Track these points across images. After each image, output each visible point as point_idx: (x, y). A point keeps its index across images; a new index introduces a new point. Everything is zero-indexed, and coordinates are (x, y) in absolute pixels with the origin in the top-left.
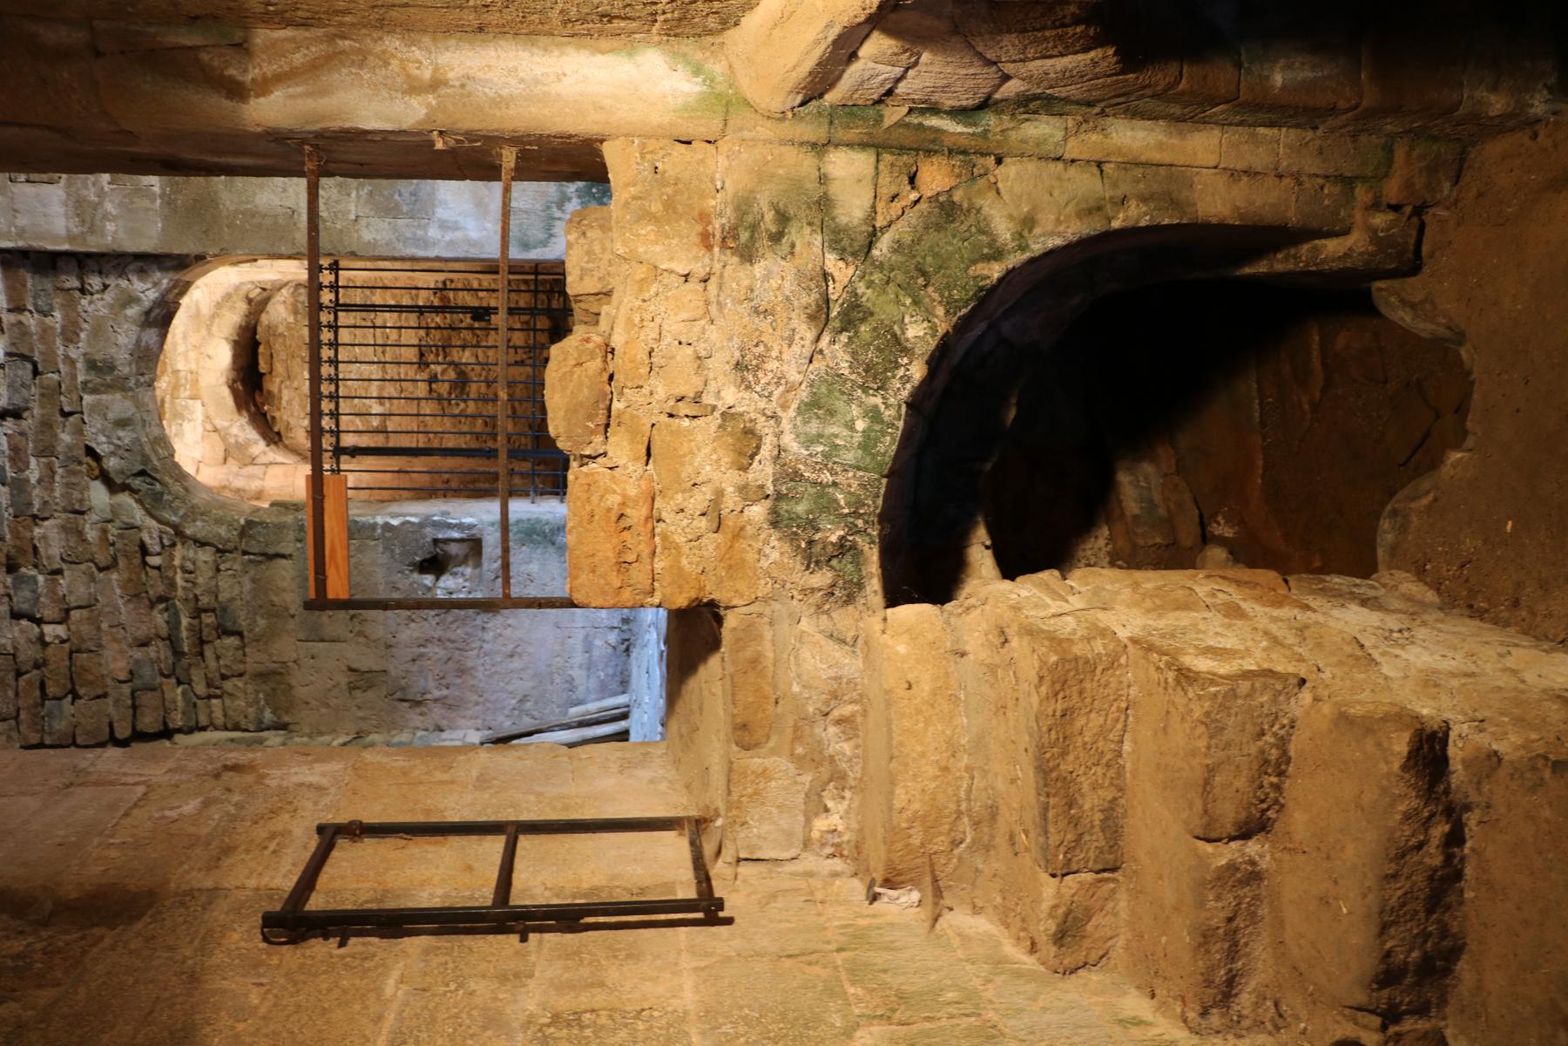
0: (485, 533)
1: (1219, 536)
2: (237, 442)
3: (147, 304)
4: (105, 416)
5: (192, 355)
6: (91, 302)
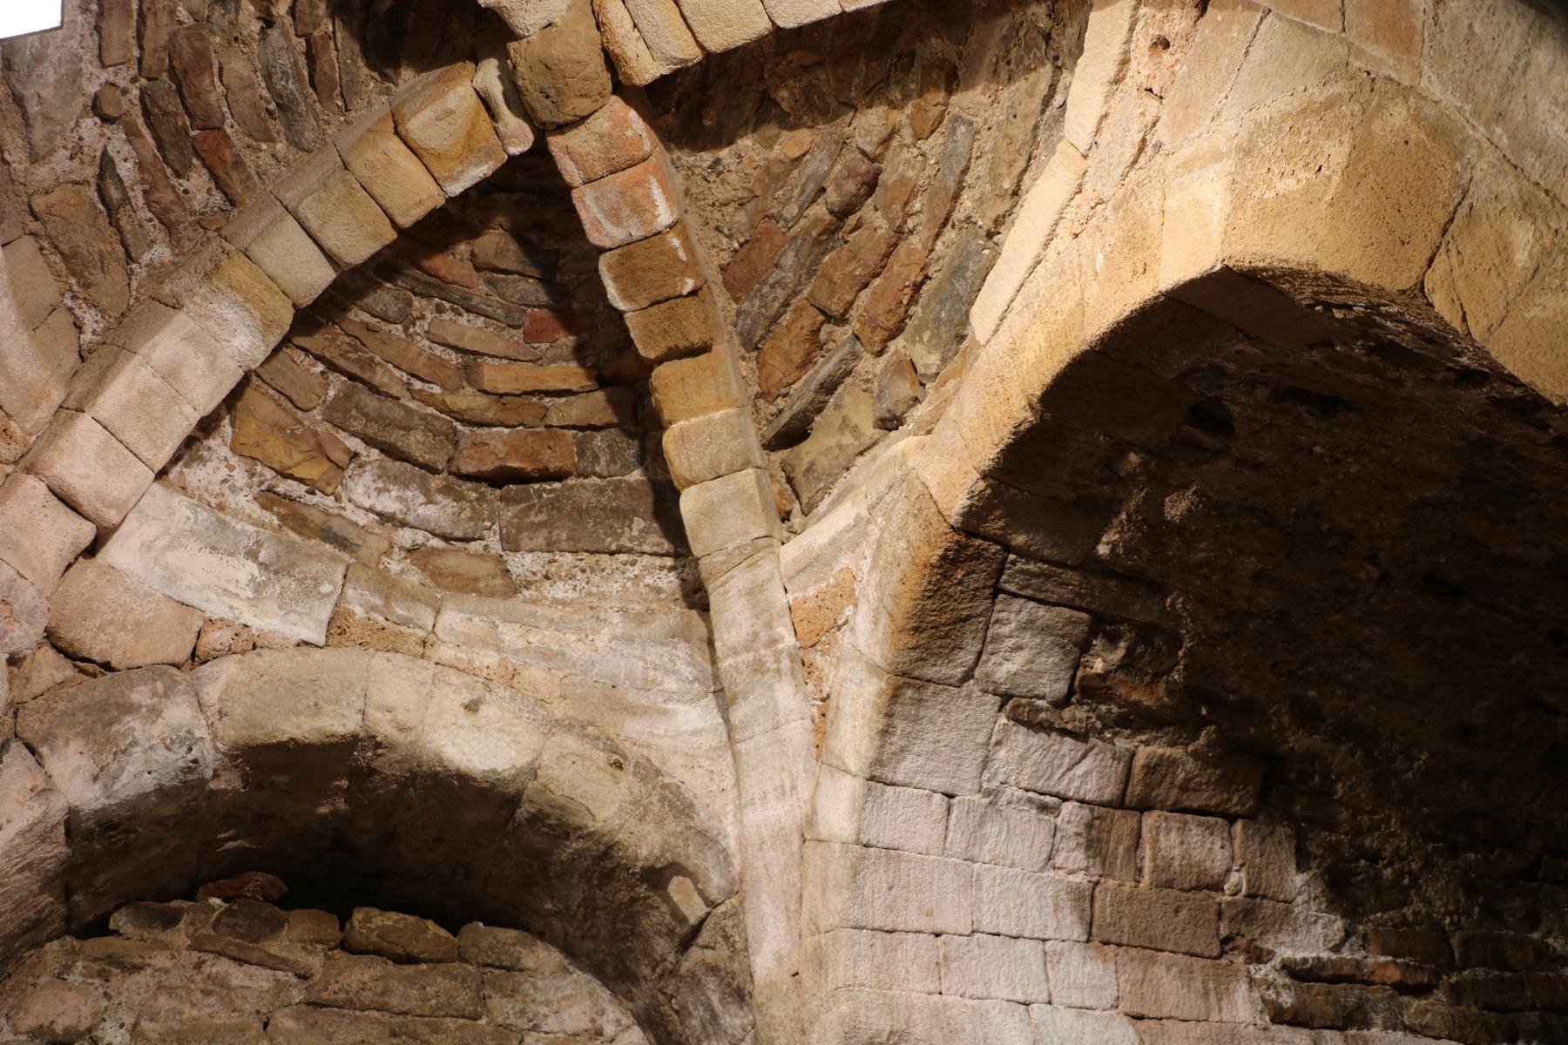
2: (129, 709)
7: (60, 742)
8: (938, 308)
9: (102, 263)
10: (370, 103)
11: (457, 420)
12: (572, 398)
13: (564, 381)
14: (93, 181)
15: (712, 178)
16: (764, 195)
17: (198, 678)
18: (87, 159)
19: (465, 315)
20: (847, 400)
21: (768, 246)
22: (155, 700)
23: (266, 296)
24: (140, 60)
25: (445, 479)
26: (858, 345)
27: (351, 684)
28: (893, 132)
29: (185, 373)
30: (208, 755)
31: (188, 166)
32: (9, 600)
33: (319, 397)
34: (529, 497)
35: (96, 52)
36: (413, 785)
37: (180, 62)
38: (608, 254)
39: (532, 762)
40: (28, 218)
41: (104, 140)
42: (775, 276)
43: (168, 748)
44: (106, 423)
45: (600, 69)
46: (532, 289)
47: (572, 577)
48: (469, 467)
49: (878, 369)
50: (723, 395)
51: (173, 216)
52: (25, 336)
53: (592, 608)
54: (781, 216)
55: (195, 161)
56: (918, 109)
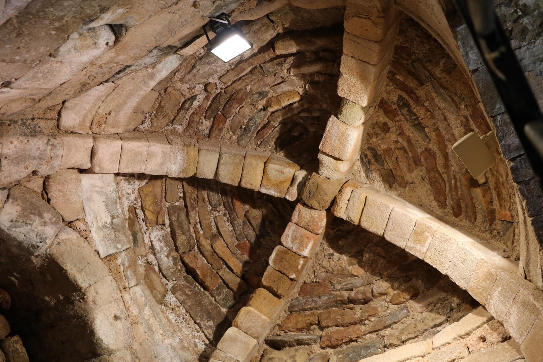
1: (234, 300)
2: (40, 215)
7: (16, 203)
8: (351, 352)
9: (165, 116)
10: (266, 150)
11: (197, 245)
12: (231, 273)
13: (234, 266)
14: (186, 98)
15: (327, 257)
16: (335, 275)
17: (64, 229)
18: (191, 92)
19: (229, 223)
20: (301, 351)
21: (323, 289)
22: (49, 221)
23: (192, 164)
24: (228, 86)
25: (177, 256)
26: (319, 340)
27: (96, 275)
28: (385, 294)
29: (153, 159)
30: (43, 249)
31: (209, 118)
32: (53, 159)
33: (173, 201)
34: (192, 284)
35: (221, 75)
36: (77, 319)
37: (236, 96)
38: (282, 246)
39: (112, 350)
40: (163, 90)
41: (199, 93)
42: (316, 299)
43: (37, 235)
44: (123, 148)
45: (329, 201)
46: (252, 235)
47: (179, 317)
48: (186, 260)
49: (318, 352)
50: (271, 313)
51: (193, 124)
52: (131, 111)
53: (174, 330)
54: (334, 285)
55: (212, 119)
56: (398, 294)
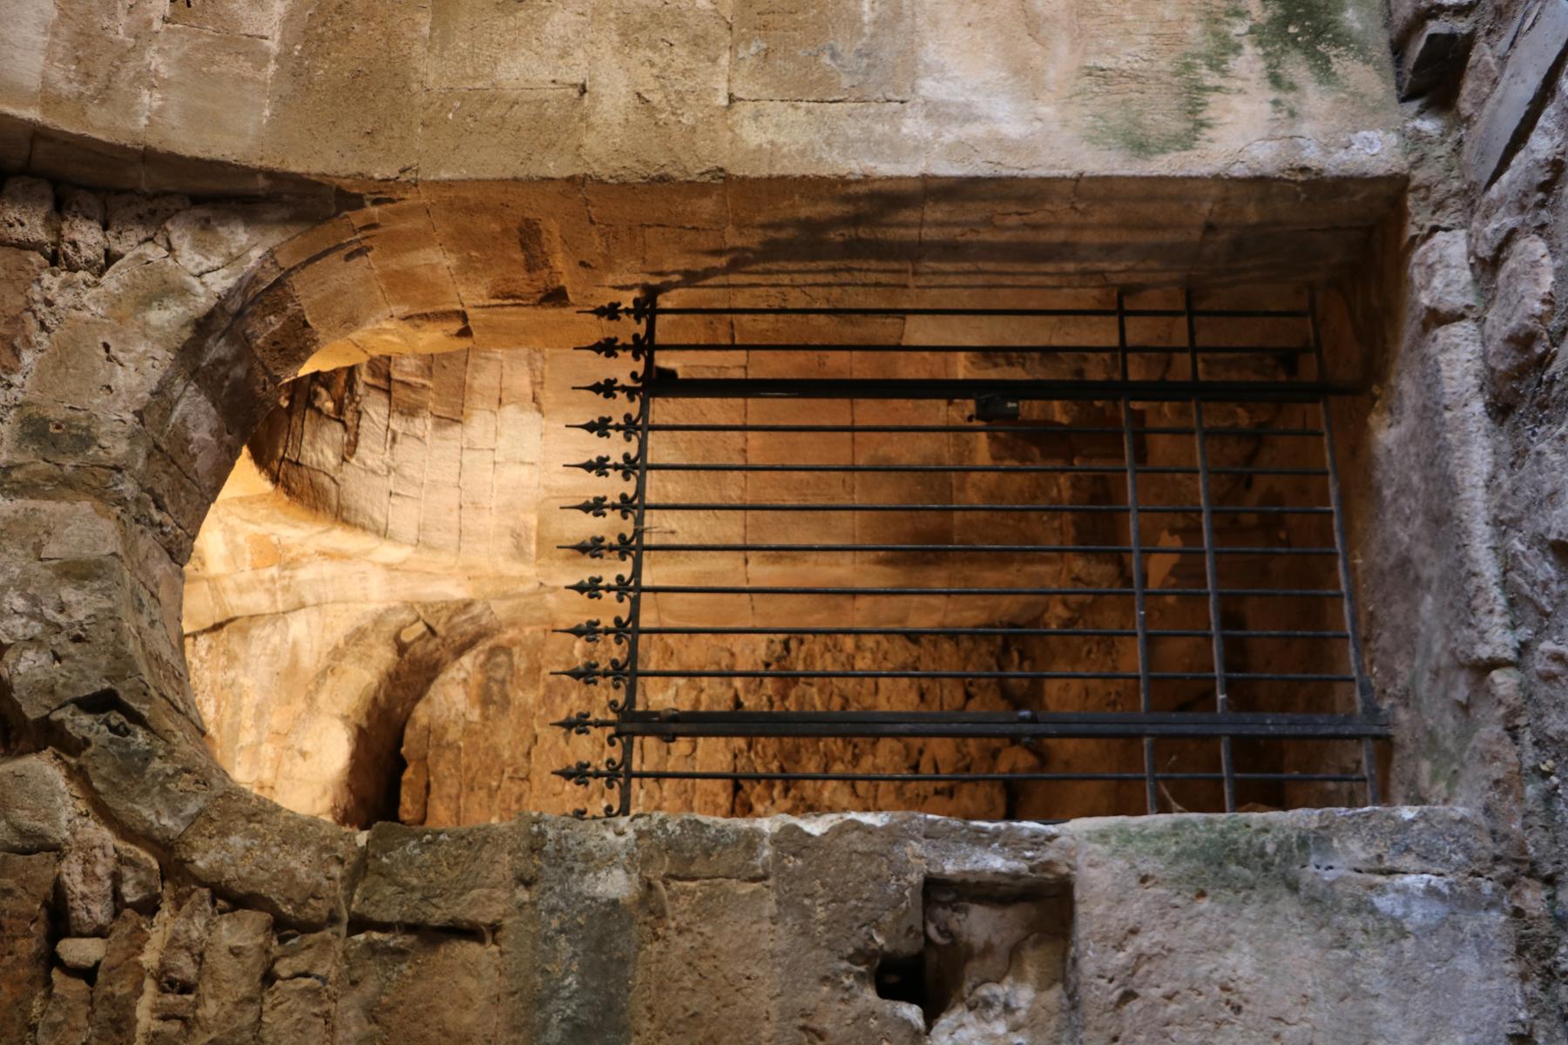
0: (1081, 861)
3: (203, 302)
4: (38, 547)
5: (268, 750)
6: (66, 285)
